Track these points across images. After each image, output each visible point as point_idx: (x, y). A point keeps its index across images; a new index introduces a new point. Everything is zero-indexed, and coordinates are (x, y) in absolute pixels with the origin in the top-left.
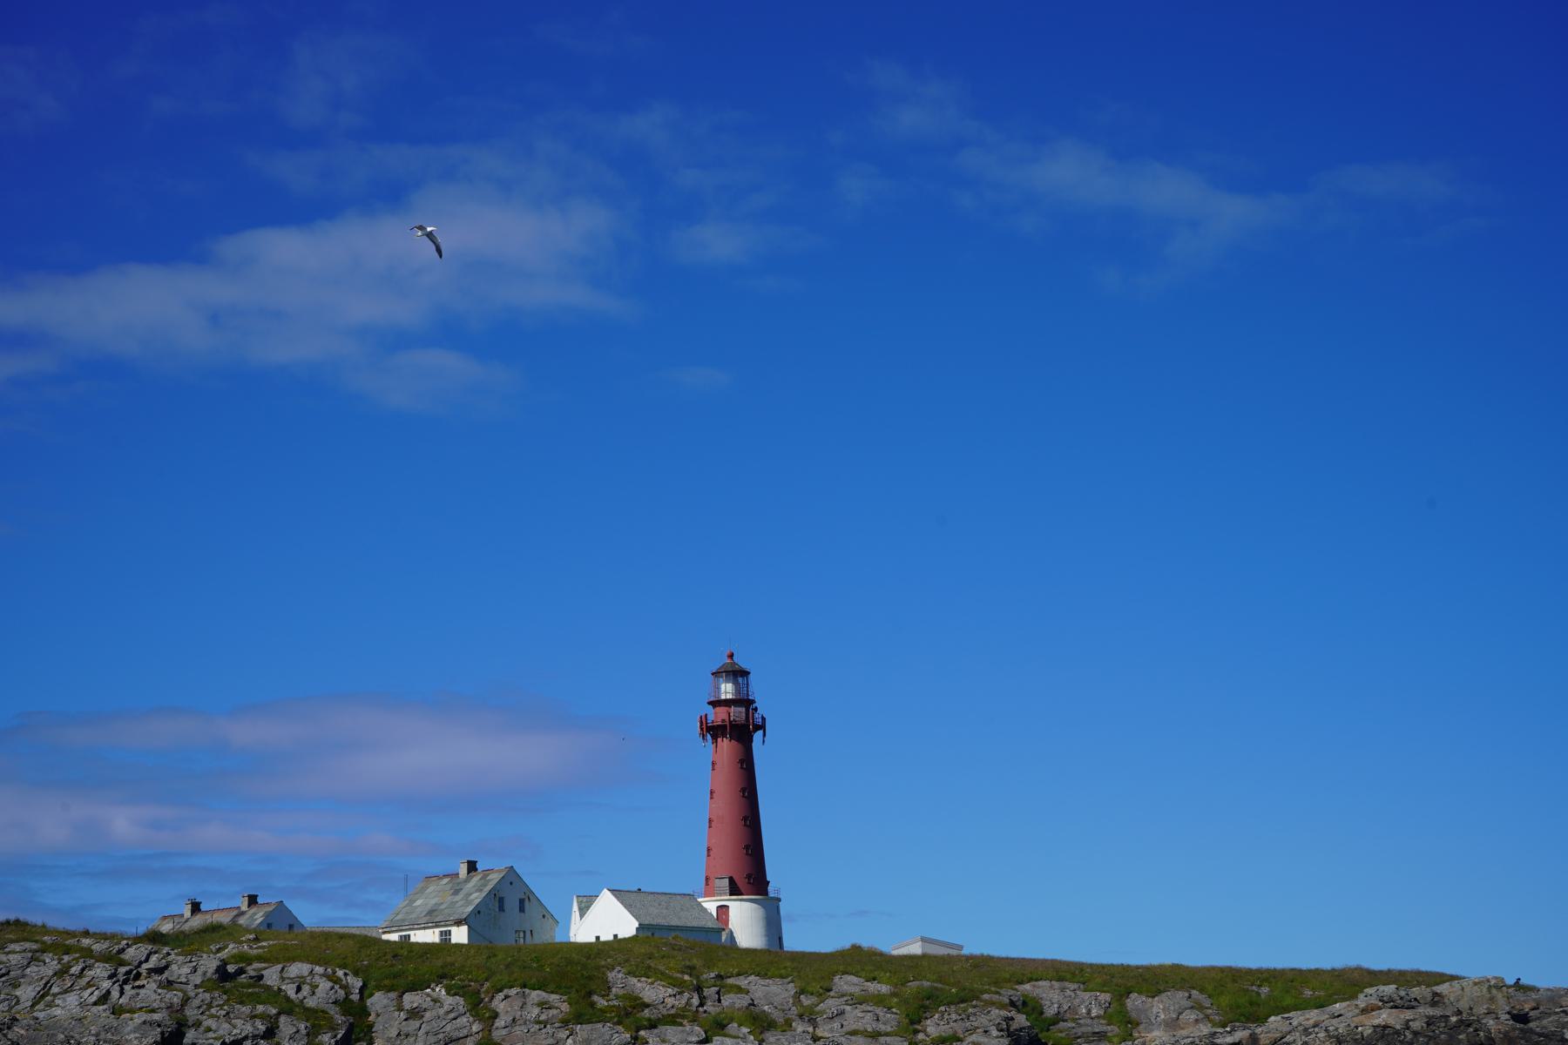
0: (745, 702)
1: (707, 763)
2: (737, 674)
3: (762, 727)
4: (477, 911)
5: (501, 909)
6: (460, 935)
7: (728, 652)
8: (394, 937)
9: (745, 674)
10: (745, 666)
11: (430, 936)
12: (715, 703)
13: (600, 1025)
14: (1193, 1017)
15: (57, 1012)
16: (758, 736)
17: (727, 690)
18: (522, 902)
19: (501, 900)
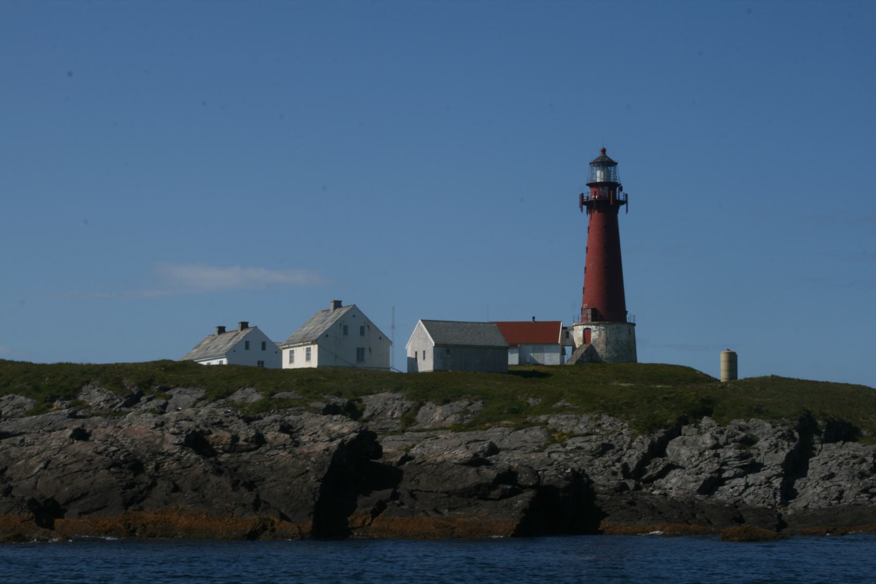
0: (612, 186)
1: (580, 227)
2: (605, 163)
3: (625, 202)
4: (326, 335)
5: (346, 333)
6: (225, 361)
7: (601, 147)
8: (205, 363)
9: (613, 164)
10: (614, 158)
11: (215, 362)
12: (593, 185)
13: (831, 444)
14: (668, 421)
15: (673, 480)
16: (622, 208)
17: (599, 176)
18: (362, 328)
19: (345, 329)
